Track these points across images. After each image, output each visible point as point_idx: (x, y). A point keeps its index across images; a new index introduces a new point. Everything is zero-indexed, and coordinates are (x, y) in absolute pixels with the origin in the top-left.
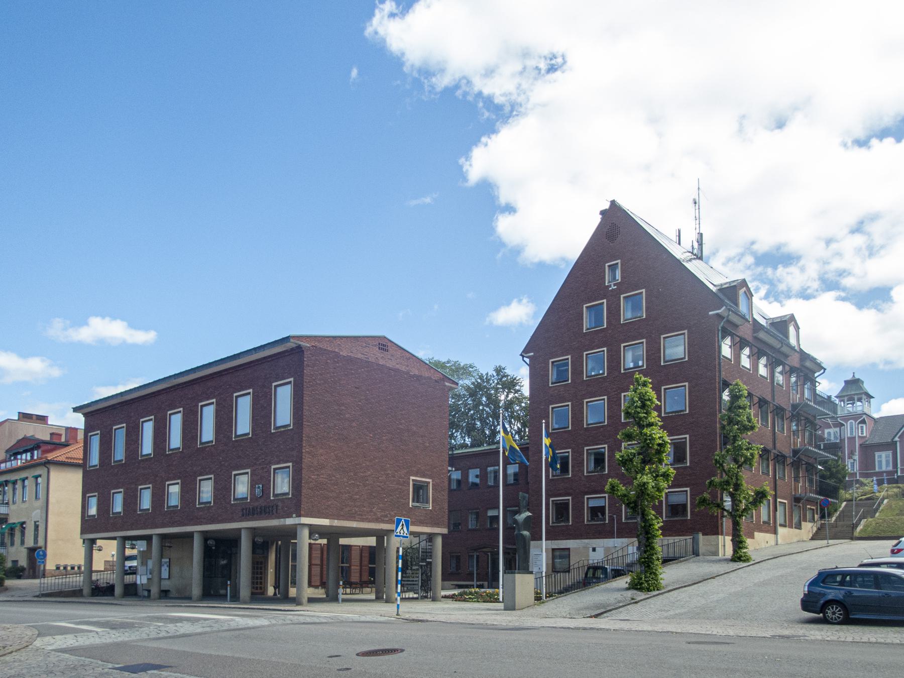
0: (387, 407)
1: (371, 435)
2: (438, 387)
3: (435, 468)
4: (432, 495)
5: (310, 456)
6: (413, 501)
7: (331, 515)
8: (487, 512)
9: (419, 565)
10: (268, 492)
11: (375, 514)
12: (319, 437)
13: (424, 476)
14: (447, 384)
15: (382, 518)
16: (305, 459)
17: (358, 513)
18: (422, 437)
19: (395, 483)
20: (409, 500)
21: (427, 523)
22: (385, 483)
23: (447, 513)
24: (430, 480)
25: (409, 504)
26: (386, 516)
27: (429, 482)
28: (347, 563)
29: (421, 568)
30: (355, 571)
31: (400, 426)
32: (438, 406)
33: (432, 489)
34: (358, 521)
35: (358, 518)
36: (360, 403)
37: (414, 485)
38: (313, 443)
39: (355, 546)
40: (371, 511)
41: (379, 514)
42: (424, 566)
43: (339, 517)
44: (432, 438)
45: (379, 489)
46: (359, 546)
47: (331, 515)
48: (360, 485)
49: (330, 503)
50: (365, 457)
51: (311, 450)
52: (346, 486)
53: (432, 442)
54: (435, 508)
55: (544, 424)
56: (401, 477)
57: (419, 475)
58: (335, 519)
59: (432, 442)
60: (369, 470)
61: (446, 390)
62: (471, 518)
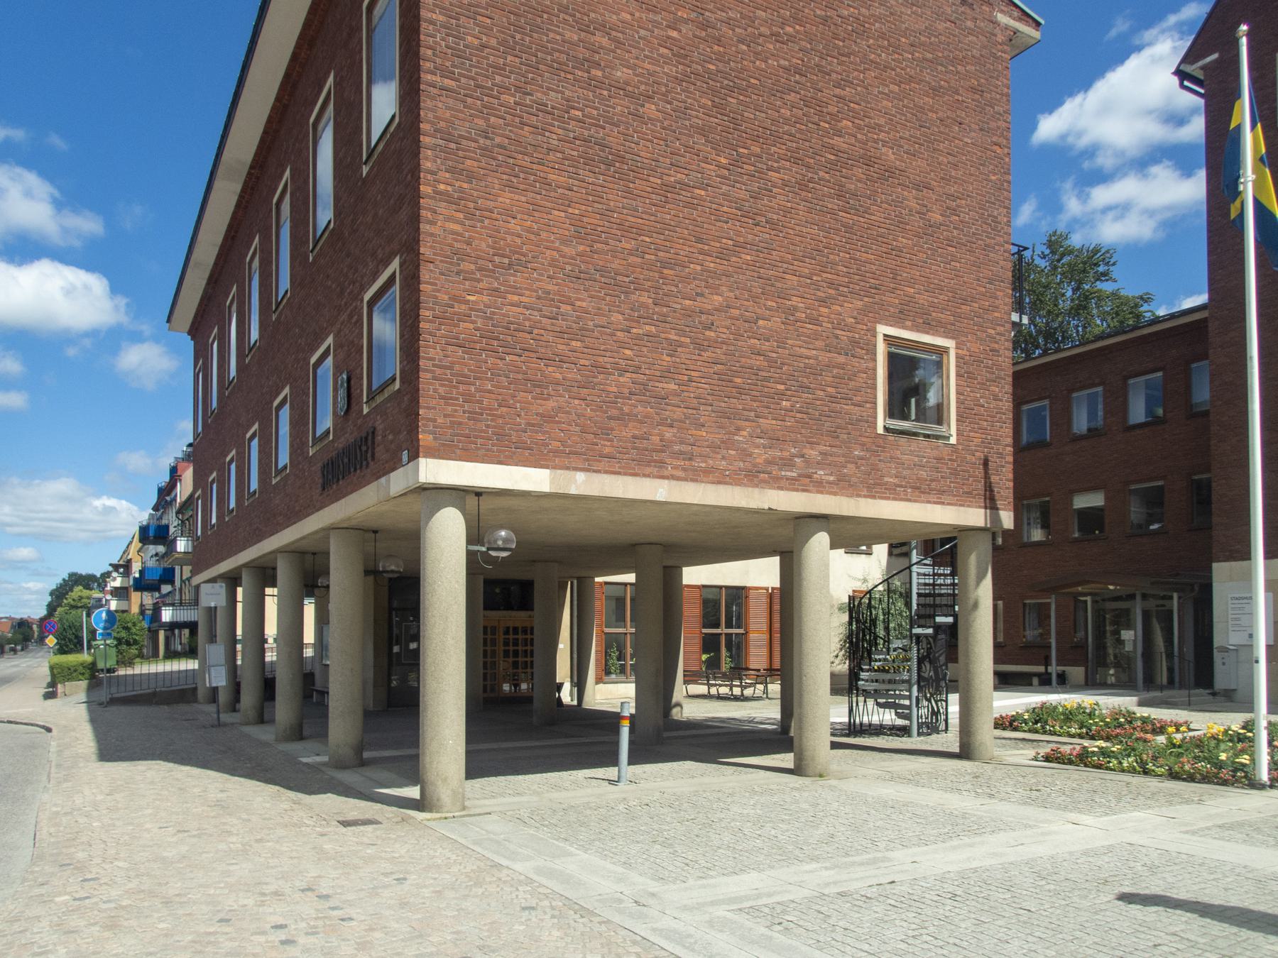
0: (782, 62)
1: (723, 161)
2: (969, 24)
3: (965, 301)
4: (958, 393)
5: (461, 216)
6: (891, 413)
7: (556, 452)
8: (1072, 500)
9: (911, 636)
10: (358, 391)
11: (745, 454)
12: (498, 140)
13: (928, 327)
14: (1003, 19)
15: (775, 470)
16: (433, 223)
17: (677, 448)
18: (918, 187)
19: (819, 344)
20: (875, 408)
21: (941, 492)
22: (782, 344)
23: (1010, 459)
24: (950, 343)
25: (875, 423)
26: (788, 463)
27: (942, 351)
28: (739, 627)
29: (918, 643)
30: (759, 643)
31: (837, 141)
32: (973, 89)
33: (958, 375)
34: (673, 477)
35: (675, 468)
36: (675, 34)
37: (892, 358)
38: (469, 162)
39: (757, 588)
40: (728, 444)
41: (760, 455)
42: (926, 636)
43: (591, 461)
44: (951, 197)
45: (758, 362)
46: (767, 589)
47: (556, 452)
48: (681, 345)
49: (551, 404)
50: (699, 240)
51: (461, 190)
52: (623, 345)
53: (954, 211)
54: (969, 439)
55: (1244, 40)
56: (842, 325)
57: (909, 323)
58: (576, 469)
59: (954, 211)
60: (716, 290)
61: (1000, 38)
62: (1029, 519)
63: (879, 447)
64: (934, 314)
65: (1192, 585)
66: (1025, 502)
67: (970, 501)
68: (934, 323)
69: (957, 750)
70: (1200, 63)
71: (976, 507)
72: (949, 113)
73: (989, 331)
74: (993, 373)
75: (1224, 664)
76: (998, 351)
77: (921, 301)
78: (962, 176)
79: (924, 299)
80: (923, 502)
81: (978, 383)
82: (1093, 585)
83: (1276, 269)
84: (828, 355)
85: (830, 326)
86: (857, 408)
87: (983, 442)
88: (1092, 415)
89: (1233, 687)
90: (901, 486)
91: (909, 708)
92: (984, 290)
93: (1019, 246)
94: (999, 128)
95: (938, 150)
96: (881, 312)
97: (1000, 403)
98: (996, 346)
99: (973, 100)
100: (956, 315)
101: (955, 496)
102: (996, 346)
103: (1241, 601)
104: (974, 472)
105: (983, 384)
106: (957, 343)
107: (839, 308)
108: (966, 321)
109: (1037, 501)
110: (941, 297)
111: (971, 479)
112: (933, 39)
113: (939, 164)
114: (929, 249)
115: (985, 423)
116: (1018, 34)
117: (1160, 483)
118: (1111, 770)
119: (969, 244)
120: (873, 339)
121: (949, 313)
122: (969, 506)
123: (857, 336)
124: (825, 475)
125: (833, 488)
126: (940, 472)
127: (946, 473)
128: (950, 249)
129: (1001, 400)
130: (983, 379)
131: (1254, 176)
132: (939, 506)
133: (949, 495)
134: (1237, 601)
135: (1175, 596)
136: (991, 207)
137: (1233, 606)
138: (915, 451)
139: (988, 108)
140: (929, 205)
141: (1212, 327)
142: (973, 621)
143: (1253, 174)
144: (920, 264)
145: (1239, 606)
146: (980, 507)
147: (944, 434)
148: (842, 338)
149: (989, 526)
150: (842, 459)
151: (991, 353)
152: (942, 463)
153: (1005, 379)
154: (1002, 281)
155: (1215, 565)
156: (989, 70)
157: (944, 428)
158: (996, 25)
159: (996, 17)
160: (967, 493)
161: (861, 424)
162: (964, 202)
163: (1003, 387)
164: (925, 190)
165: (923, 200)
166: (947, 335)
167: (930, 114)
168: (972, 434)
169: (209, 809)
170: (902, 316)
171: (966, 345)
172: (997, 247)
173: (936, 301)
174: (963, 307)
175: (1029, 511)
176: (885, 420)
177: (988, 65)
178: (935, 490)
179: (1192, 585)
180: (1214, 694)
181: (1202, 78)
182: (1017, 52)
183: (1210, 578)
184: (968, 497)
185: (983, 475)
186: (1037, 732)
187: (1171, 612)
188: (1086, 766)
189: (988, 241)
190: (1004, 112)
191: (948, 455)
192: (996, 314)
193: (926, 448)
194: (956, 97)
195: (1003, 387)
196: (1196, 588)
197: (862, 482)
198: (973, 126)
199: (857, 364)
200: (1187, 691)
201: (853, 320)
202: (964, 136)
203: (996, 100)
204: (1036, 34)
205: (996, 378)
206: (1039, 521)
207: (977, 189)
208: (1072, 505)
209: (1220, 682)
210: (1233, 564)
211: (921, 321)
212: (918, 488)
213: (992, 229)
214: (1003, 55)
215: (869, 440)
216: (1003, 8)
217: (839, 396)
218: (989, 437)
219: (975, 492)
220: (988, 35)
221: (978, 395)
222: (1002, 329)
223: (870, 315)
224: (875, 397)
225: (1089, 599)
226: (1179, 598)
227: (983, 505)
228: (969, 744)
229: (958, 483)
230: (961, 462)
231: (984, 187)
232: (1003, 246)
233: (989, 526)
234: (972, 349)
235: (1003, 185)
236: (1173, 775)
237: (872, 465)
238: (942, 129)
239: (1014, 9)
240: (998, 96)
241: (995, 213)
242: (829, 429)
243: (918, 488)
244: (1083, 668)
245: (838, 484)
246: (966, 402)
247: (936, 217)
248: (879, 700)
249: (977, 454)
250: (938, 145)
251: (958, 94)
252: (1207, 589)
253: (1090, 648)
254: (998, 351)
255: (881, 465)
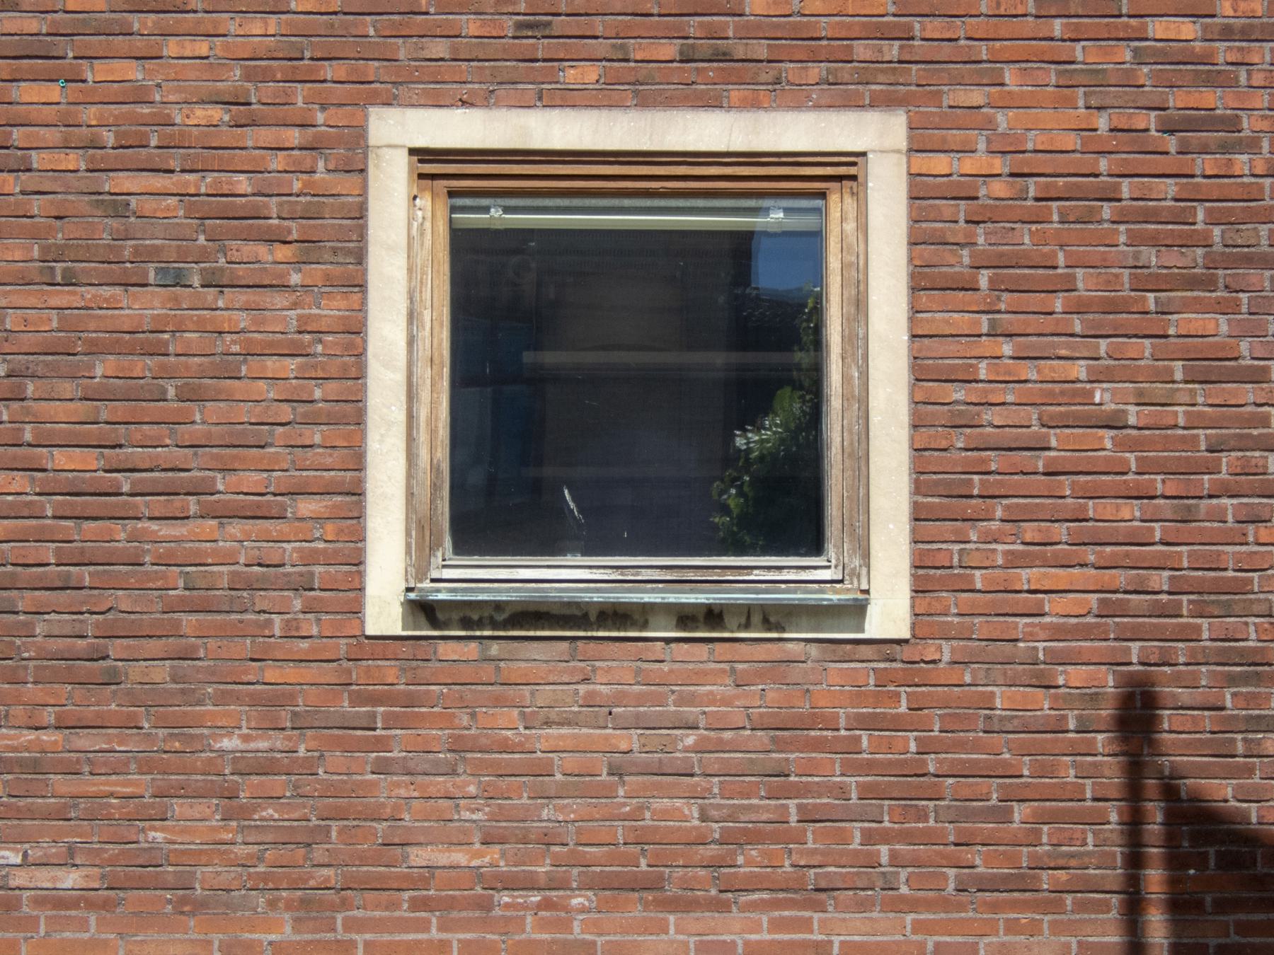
63: (375, 700)
67: (1012, 928)
76: (1232, 124)
81: (1078, 309)
83: (121, 953)
84: (62, 297)
85: (73, 160)
86: (236, 528)
90: (530, 885)
96: (403, 50)
98: (1210, 98)
102: (1210, 98)
107: (134, 72)
120: (345, 184)
123: (243, 183)
124: (26, 863)
125: (83, 925)
127: (842, 792)
130: (1111, 284)
133: (863, 906)
138: (620, 699)
148: (149, 205)
150: (139, 783)
151: (1172, 143)
152: (818, 745)
161: (263, 600)
168: (1026, 577)
169: (79, 691)
170: (542, 47)
176: (419, 565)
184: (995, 907)
193: (700, 677)
197: (263, 884)
199: (243, 320)
201: (217, 114)
205: (1212, 264)
212: (651, 885)
215: (312, 672)
217: (125, 482)
218: (1161, 579)
221: (1079, 370)
223: (329, 70)
224: (357, 462)
229: (929, 838)
237: (331, 791)
242: (56, 645)
243: (651, 885)
245: (107, 905)
254: (1232, 124)
255: (390, 790)
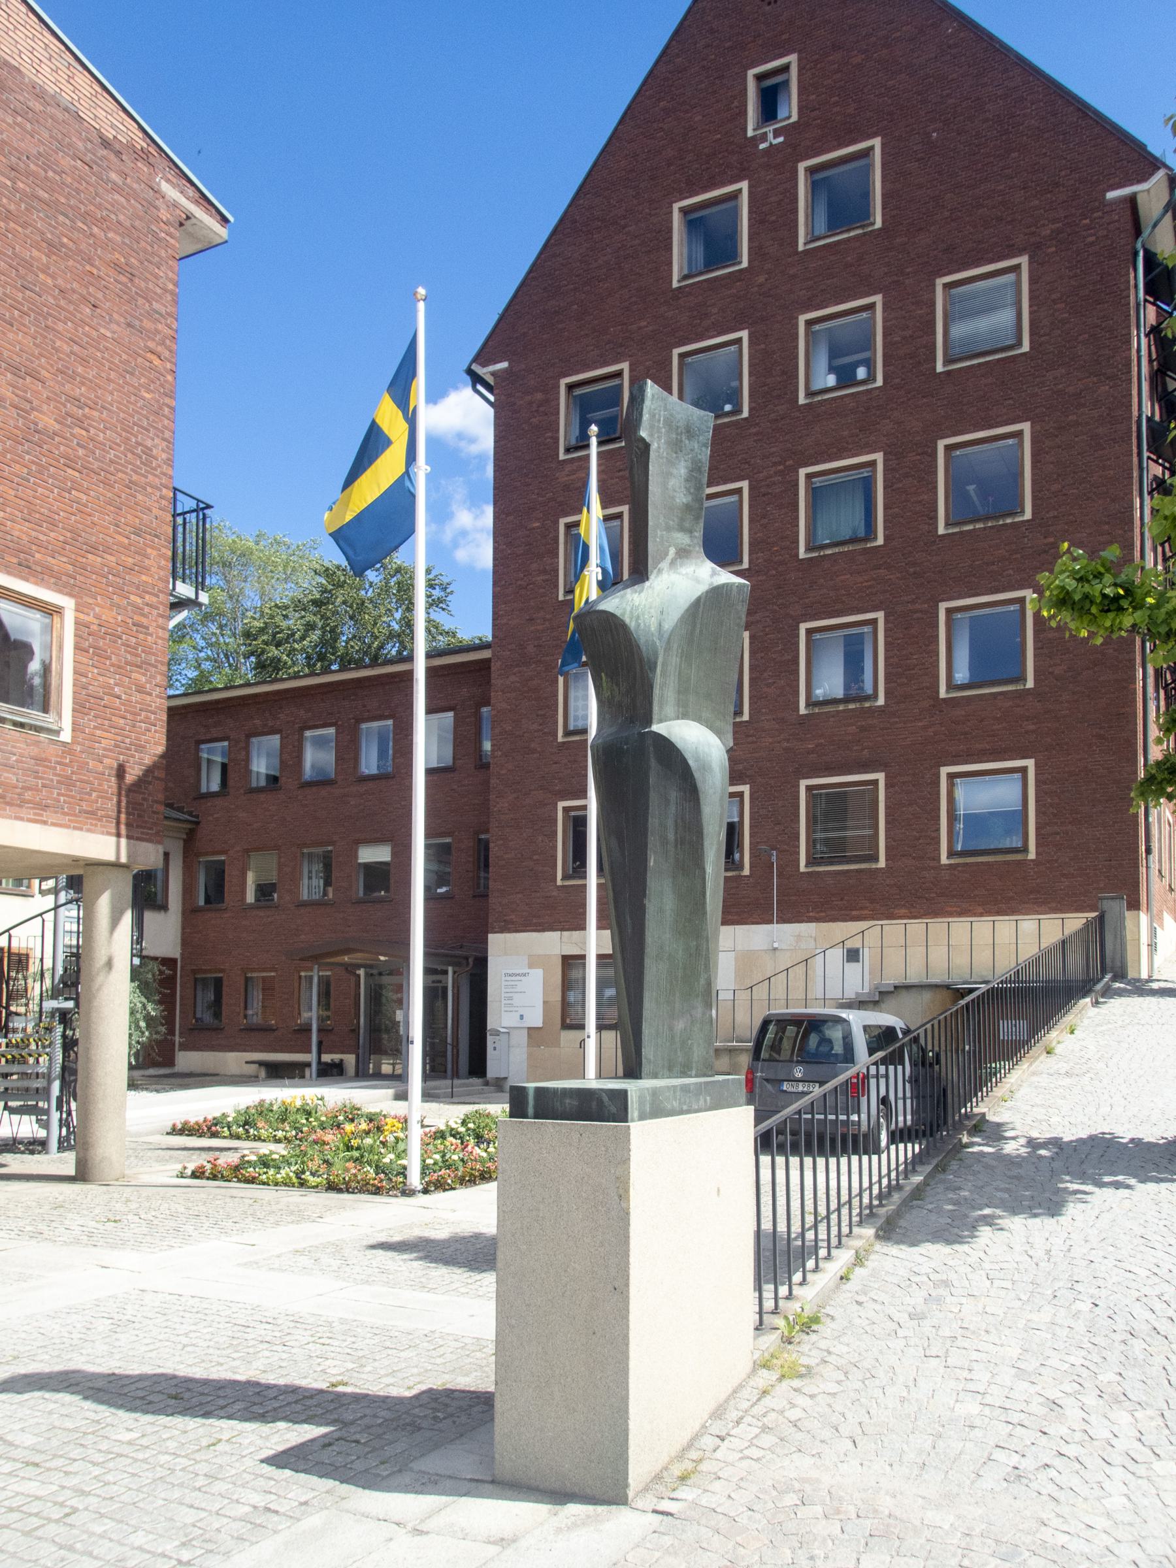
3: (93, 549)
33: (77, 648)
59: (80, 422)
62: (310, 872)
64: (37, 555)
65: (467, 958)
66: (305, 851)
67: (91, 824)
68: (39, 569)
69: (72, 1172)
70: (492, 368)
71: (103, 833)
72: (75, 285)
73: (132, 597)
74: (137, 655)
75: (495, 1049)
76: (147, 628)
77: (16, 533)
78: (93, 376)
79: (21, 531)
80: (10, 817)
81: (112, 665)
82: (359, 955)
87: (116, 746)
88: (382, 754)
89: (503, 1076)
91: (47, 1112)
92: (126, 541)
93: (198, 501)
94: (157, 331)
95: (54, 329)
97: (148, 698)
99: (116, 280)
100: (78, 564)
101: (67, 814)
103: (513, 978)
104: (100, 785)
105: (119, 667)
106: (77, 604)
108: (94, 577)
109: (319, 850)
110: (52, 534)
111: (94, 794)
112: (50, 174)
113: (57, 350)
114: (33, 462)
115: (122, 721)
116: (193, 221)
117: (448, 840)
118: (264, 1183)
119: (102, 473)
121: (64, 559)
122: (89, 830)
126: (42, 778)
127: (52, 780)
128: (70, 471)
129: (150, 694)
131: (429, 469)
132: (37, 826)
133: (56, 812)
134: (510, 978)
135: (450, 970)
136: (142, 433)
137: (507, 983)
139: (140, 301)
140: (36, 403)
141: (495, 666)
142: (98, 990)
143: (427, 464)
144: (16, 480)
145: (513, 983)
146: (109, 834)
147: (50, 726)
149: (123, 860)
151: (135, 628)
152: (47, 767)
153: (156, 667)
154: (156, 536)
155: (490, 936)
156: (145, 251)
157: (49, 720)
158: (158, 196)
159: (159, 184)
160: (87, 812)
162: (96, 414)
163: (154, 677)
164: (28, 379)
165: (26, 392)
166: (61, 588)
167: (42, 276)
168: (98, 732)
171: (93, 609)
172: (149, 489)
173: (42, 537)
174: (90, 556)
175: (310, 862)
177: (143, 244)
178: (29, 802)
179: (467, 958)
180: (487, 1084)
181: (492, 384)
182: (199, 247)
183: (486, 950)
185: (115, 790)
186: (238, 1137)
187: (445, 989)
188: (239, 1181)
189: (135, 477)
190: (168, 314)
191: (57, 756)
192: (144, 578)
194: (88, 268)
195: (151, 677)
196: (471, 960)
198: (115, 316)
200: (449, 1082)
202: (99, 324)
203: (155, 293)
204: (223, 232)
206: (321, 875)
207: (120, 403)
208: (356, 857)
209: (492, 1071)
210: (508, 936)
211: (15, 560)
213: (142, 463)
214: (168, 238)
216: (170, 177)
218: (128, 740)
219: (100, 813)
220: (144, 203)
221: (112, 681)
222: (155, 599)
225: (361, 972)
226: (454, 973)
227: (114, 831)
228: (86, 1161)
229: (73, 797)
230: (80, 768)
231: (131, 403)
232: (160, 490)
233: (123, 860)
234: (104, 617)
235: (161, 408)
236: (332, 1187)
238: (62, 303)
239: (188, 185)
240: (159, 291)
241: (149, 443)
244: (354, 1056)
246: (91, 687)
247: (48, 421)
248: (10, 1104)
249: (106, 761)
250: (55, 323)
251: (92, 265)
252: (481, 963)
253: (362, 1031)
254: (147, 628)
